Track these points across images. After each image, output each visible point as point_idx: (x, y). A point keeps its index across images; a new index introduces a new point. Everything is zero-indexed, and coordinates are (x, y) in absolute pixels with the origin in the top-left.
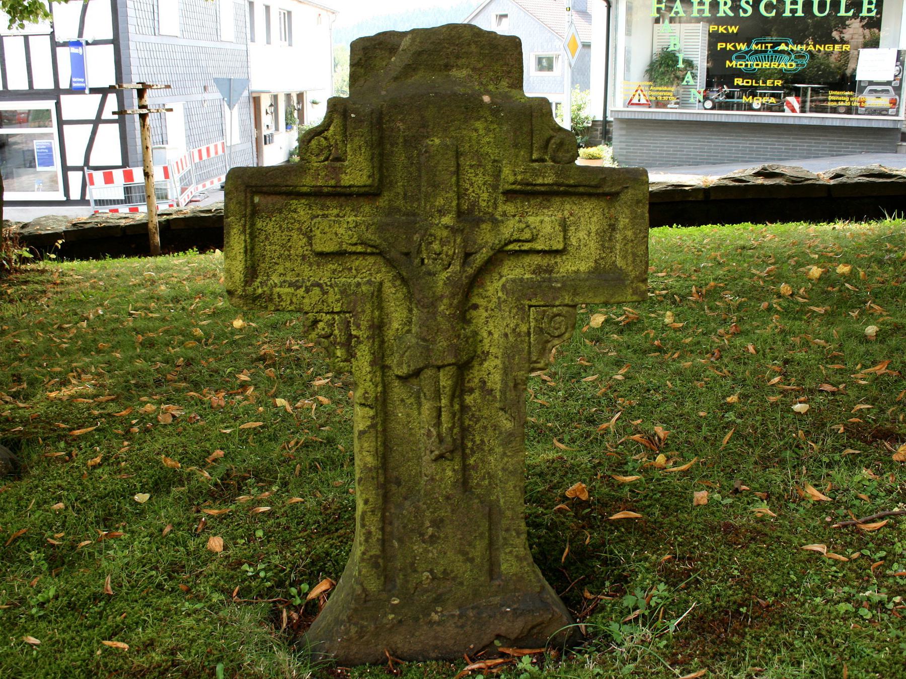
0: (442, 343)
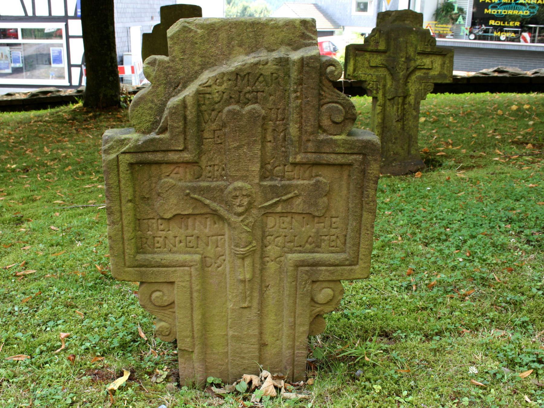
0: (400, 91)
